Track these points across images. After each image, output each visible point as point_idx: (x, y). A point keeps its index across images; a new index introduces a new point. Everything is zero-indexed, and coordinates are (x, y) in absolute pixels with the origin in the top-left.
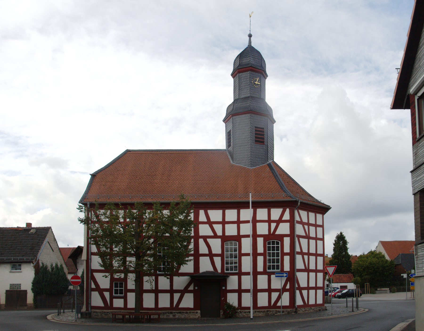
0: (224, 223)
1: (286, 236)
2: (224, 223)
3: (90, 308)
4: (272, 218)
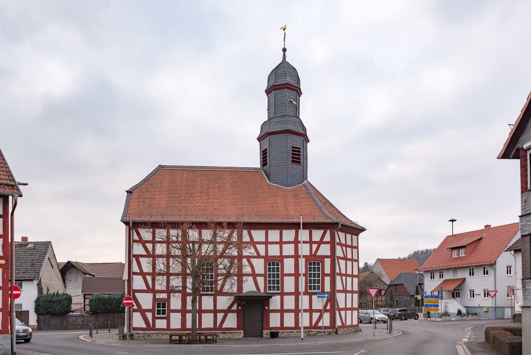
1: (327, 257)
2: (267, 243)
3: (132, 330)
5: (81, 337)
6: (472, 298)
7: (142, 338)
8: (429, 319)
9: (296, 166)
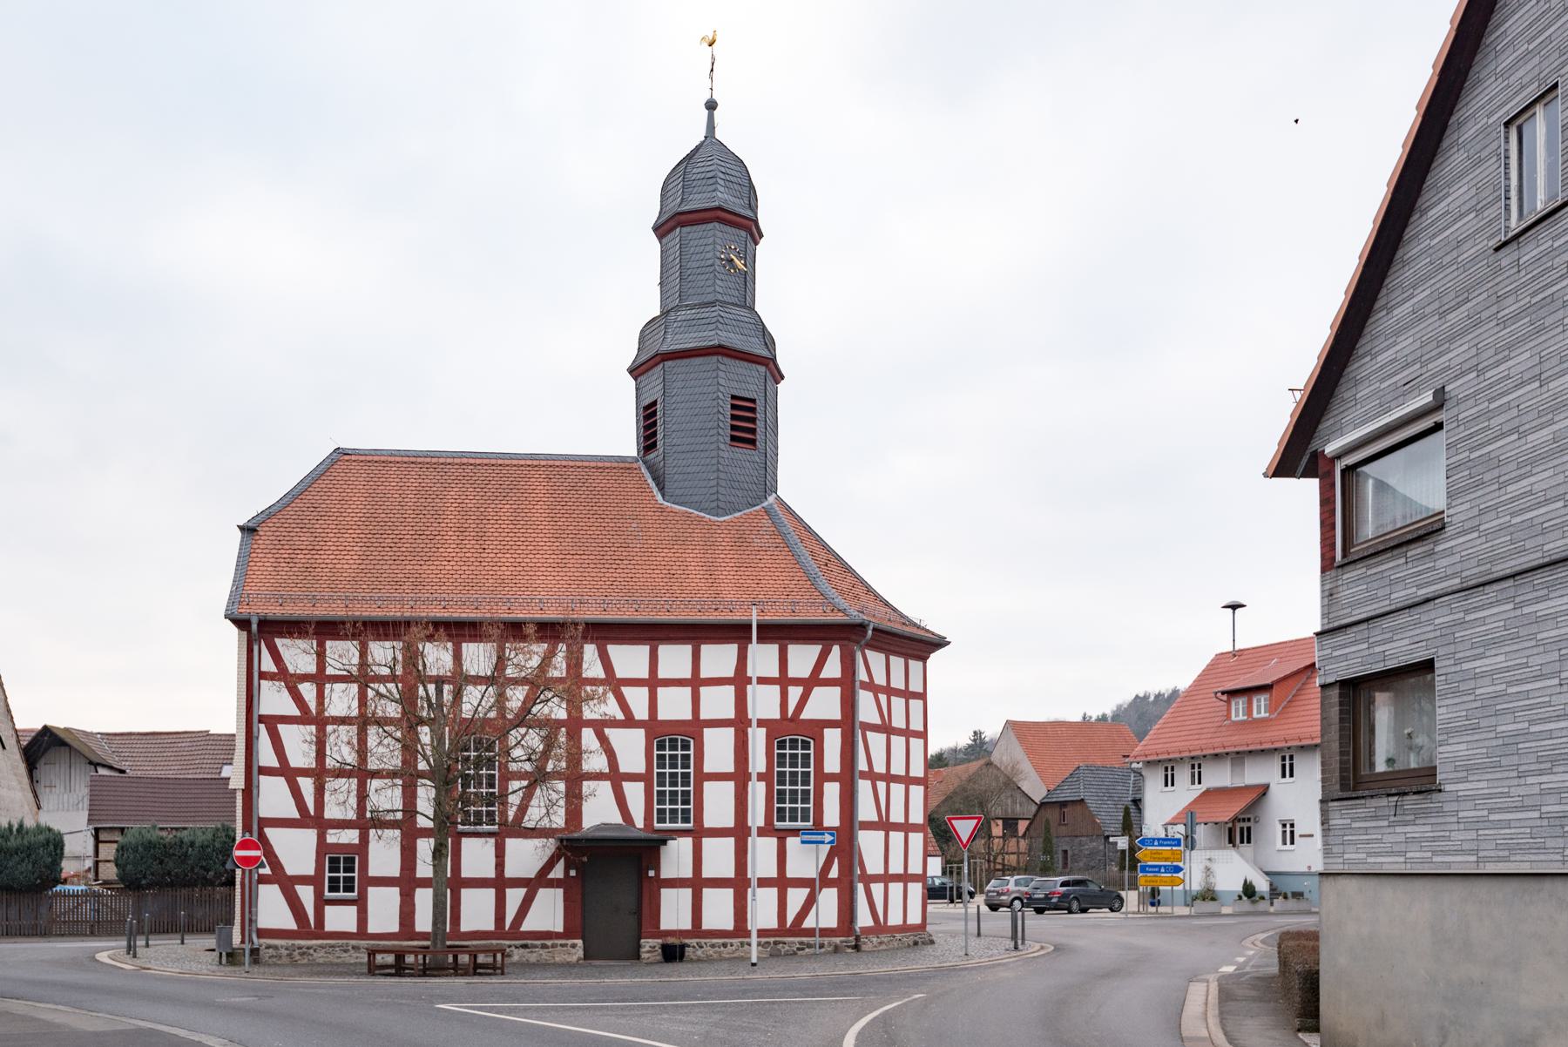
0: (653, 683)
1: (831, 724)
2: (653, 683)
3: (254, 937)
4: (792, 673)
5: (103, 957)
6: (1289, 846)
7: (285, 960)
8: (1152, 909)
9: (742, 453)
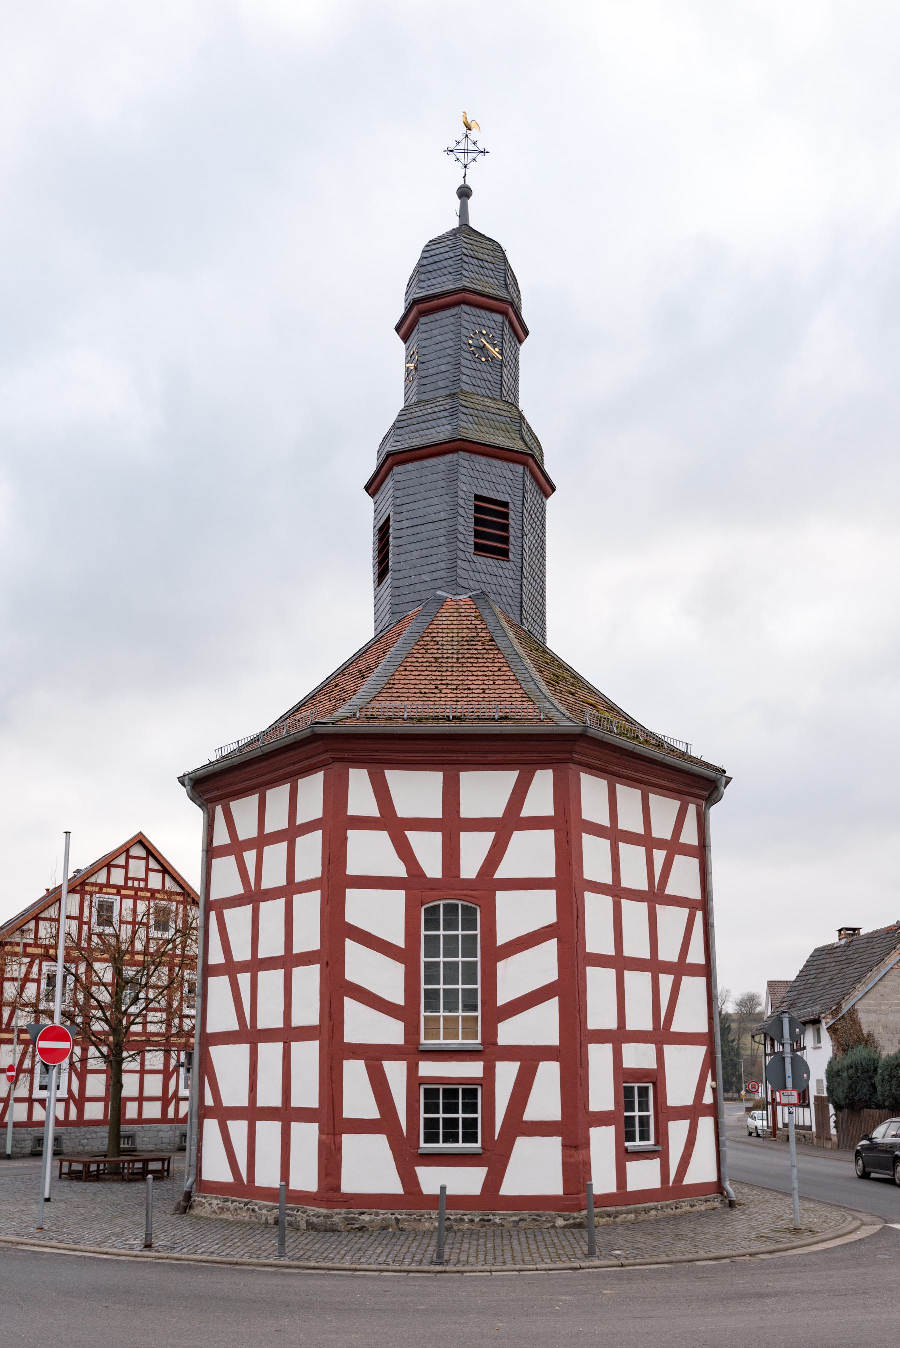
9: (486, 563)
